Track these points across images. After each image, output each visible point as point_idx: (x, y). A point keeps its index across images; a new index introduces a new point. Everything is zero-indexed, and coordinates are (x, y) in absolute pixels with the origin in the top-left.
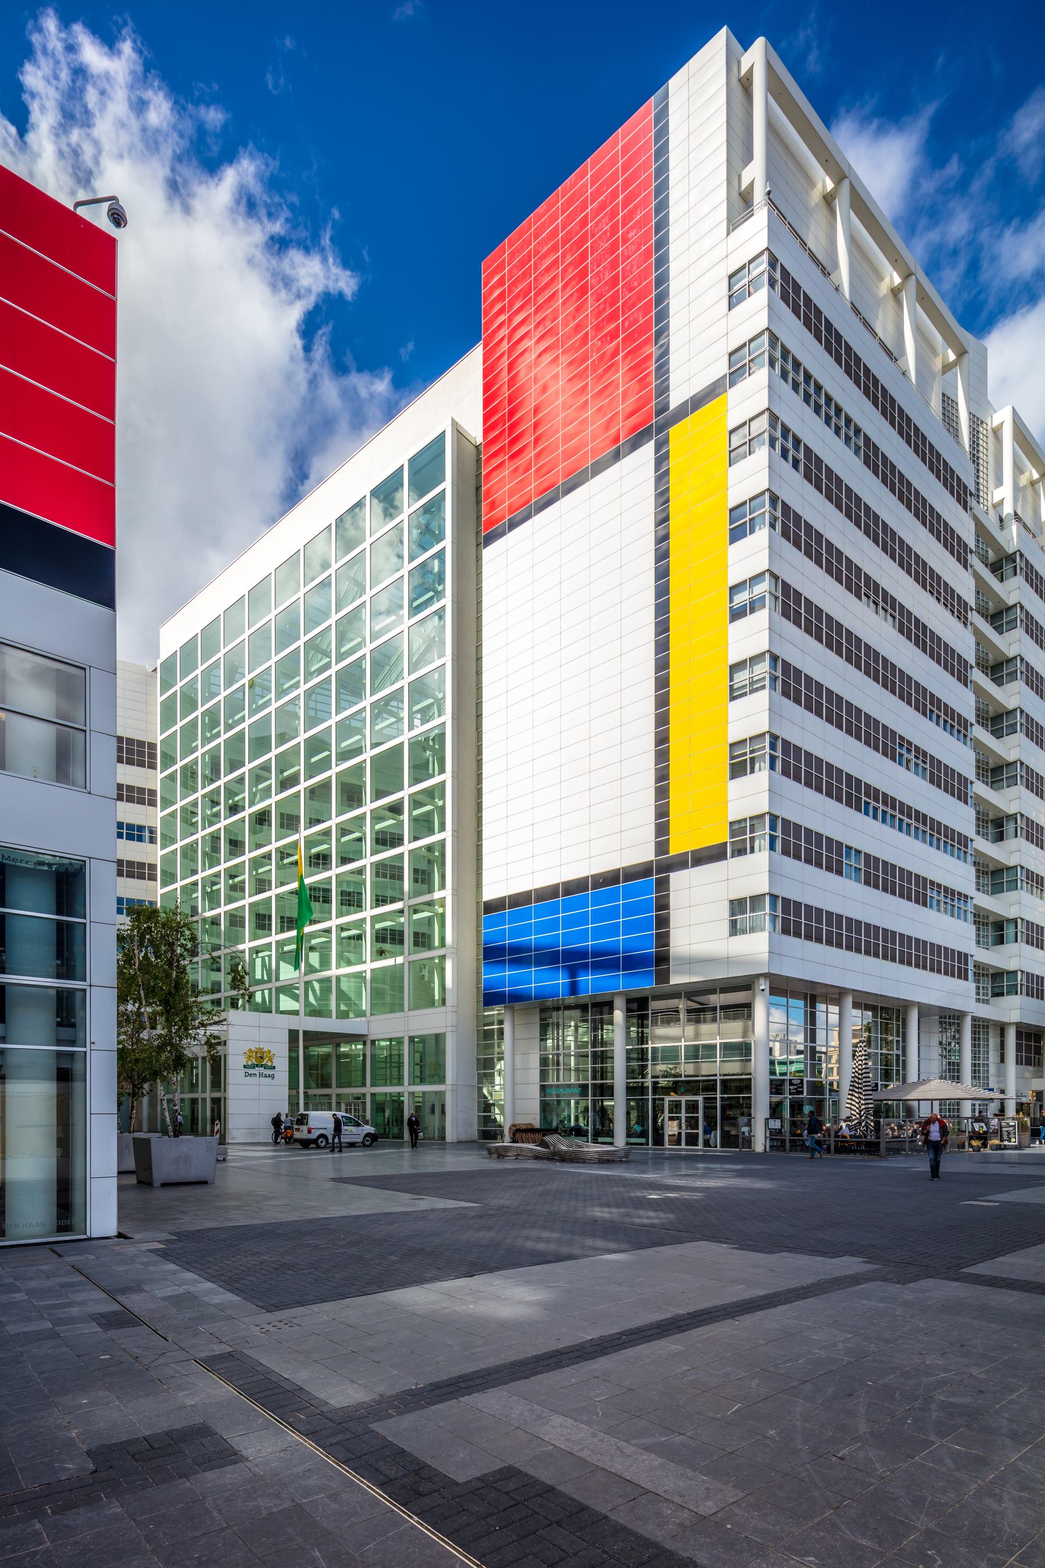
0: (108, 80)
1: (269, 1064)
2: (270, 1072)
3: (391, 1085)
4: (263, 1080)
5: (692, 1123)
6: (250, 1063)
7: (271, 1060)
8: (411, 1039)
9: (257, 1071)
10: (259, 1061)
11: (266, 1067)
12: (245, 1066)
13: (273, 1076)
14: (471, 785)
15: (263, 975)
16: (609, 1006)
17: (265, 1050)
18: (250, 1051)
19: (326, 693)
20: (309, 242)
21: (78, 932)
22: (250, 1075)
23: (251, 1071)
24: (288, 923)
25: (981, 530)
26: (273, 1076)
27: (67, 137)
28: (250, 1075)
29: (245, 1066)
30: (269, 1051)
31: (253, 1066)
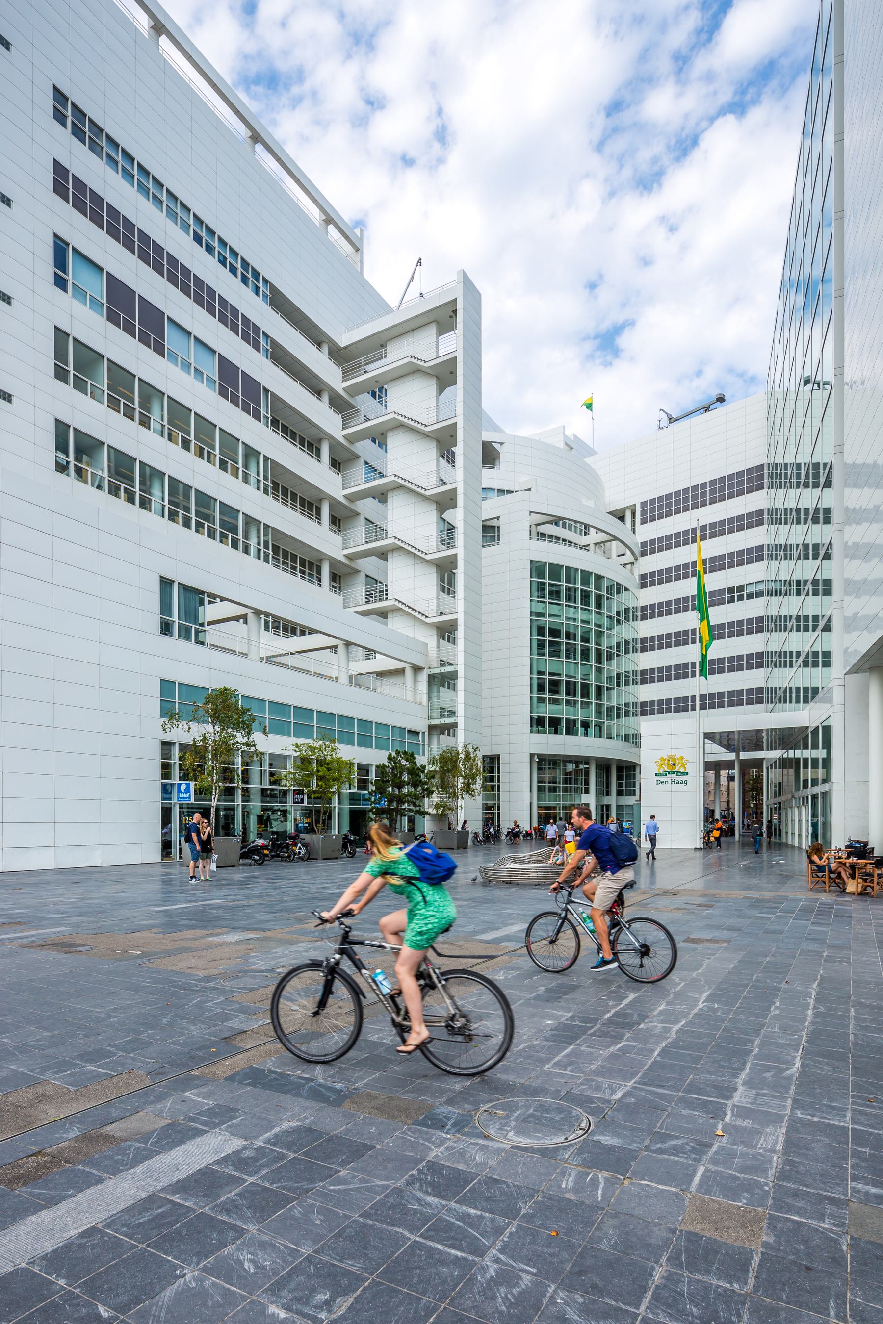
1: (682, 770)
2: (684, 778)
4: (675, 786)
5: (374, 981)
6: (662, 771)
7: (683, 766)
8: (694, 709)
9: (669, 778)
10: (672, 770)
11: (677, 773)
12: (656, 775)
17: (678, 756)
18: (662, 759)
20: (863, 871)
23: (662, 779)
24: (486, 1298)
25: (403, 877)
27: (455, 919)
29: (656, 775)
30: (682, 758)
31: (666, 774)
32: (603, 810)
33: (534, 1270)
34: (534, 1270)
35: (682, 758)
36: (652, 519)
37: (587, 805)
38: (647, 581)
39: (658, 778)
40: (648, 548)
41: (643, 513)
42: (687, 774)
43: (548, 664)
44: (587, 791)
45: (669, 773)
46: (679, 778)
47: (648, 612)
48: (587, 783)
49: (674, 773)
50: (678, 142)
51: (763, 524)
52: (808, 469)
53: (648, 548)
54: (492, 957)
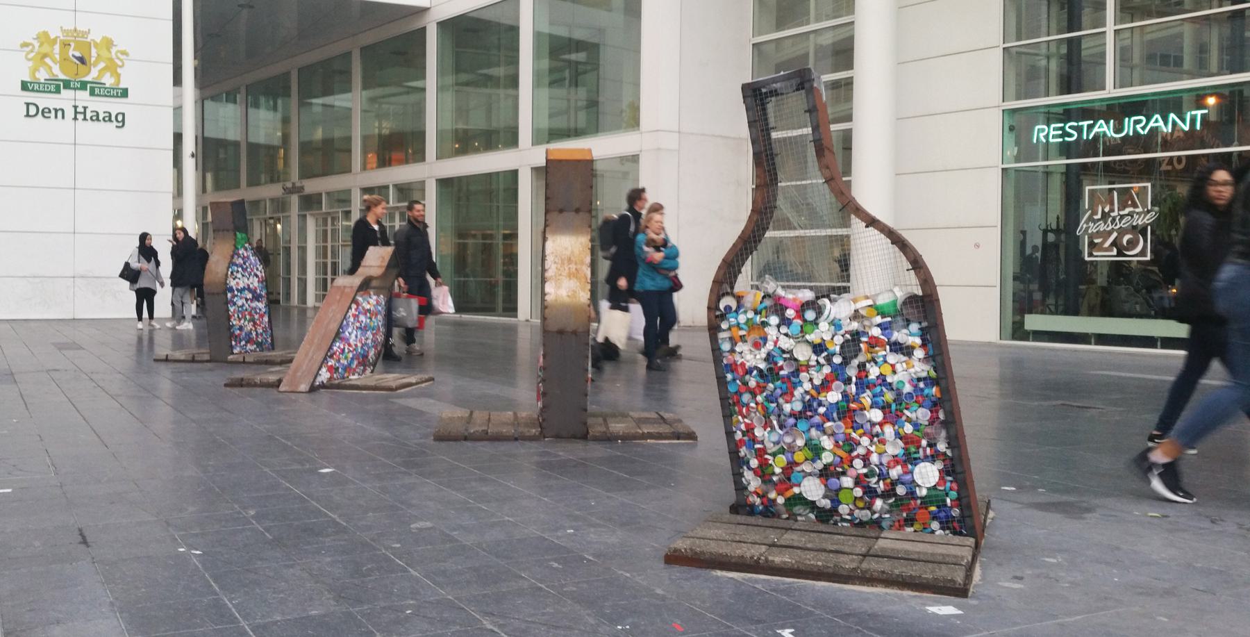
0: (798, 206)
1: (108, 81)
2: (114, 106)
3: (790, 138)
4: (88, 129)
6: (42, 76)
7: (112, 67)
9: (66, 100)
11: (95, 89)
12: (25, 86)
13: (121, 121)
14: (927, 573)
15: (1169, 343)
16: (350, 53)
17: (95, 36)
18: (44, 38)
19: (1044, 29)
21: (1012, 89)
22: (45, 113)
23: (45, 101)
26: (121, 121)
28: (45, 113)
29: (25, 86)
30: (109, 43)
31: (56, 86)
33: (1198, 127)
34: (1198, 127)
42: (125, 93)
43: (228, 121)
45: (67, 85)
49: (83, 86)
50: (738, 403)
54: (674, 558)
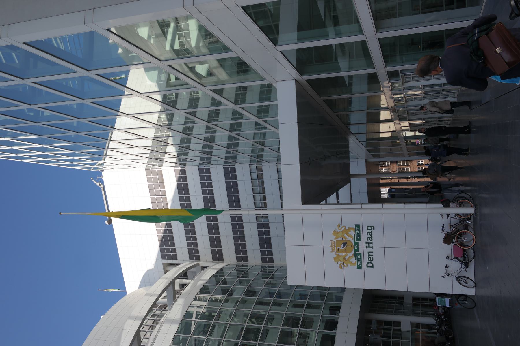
1: (353, 233)
4: (376, 242)
6: (354, 260)
7: (347, 231)
9: (364, 251)
10: (352, 245)
11: (357, 238)
12: (359, 268)
18: (337, 259)
23: (365, 260)
29: (359, 268)
31: (358, 255)
32: (418, 305)
35: (335, 232)
36: (174, 251)
37: (412, 324)
38: (218, 257)
39: (364, 265)
40: (194, 255)
41: (169, 258)
42: (357, 226)
44: (399, 324)
45: (357, 250)
46: (364, 236)
47: (242, 255)
48: (388, 323)
49: (356, 244)
51: (209, 169)
52: (233, 153)
53: (194, 255)
